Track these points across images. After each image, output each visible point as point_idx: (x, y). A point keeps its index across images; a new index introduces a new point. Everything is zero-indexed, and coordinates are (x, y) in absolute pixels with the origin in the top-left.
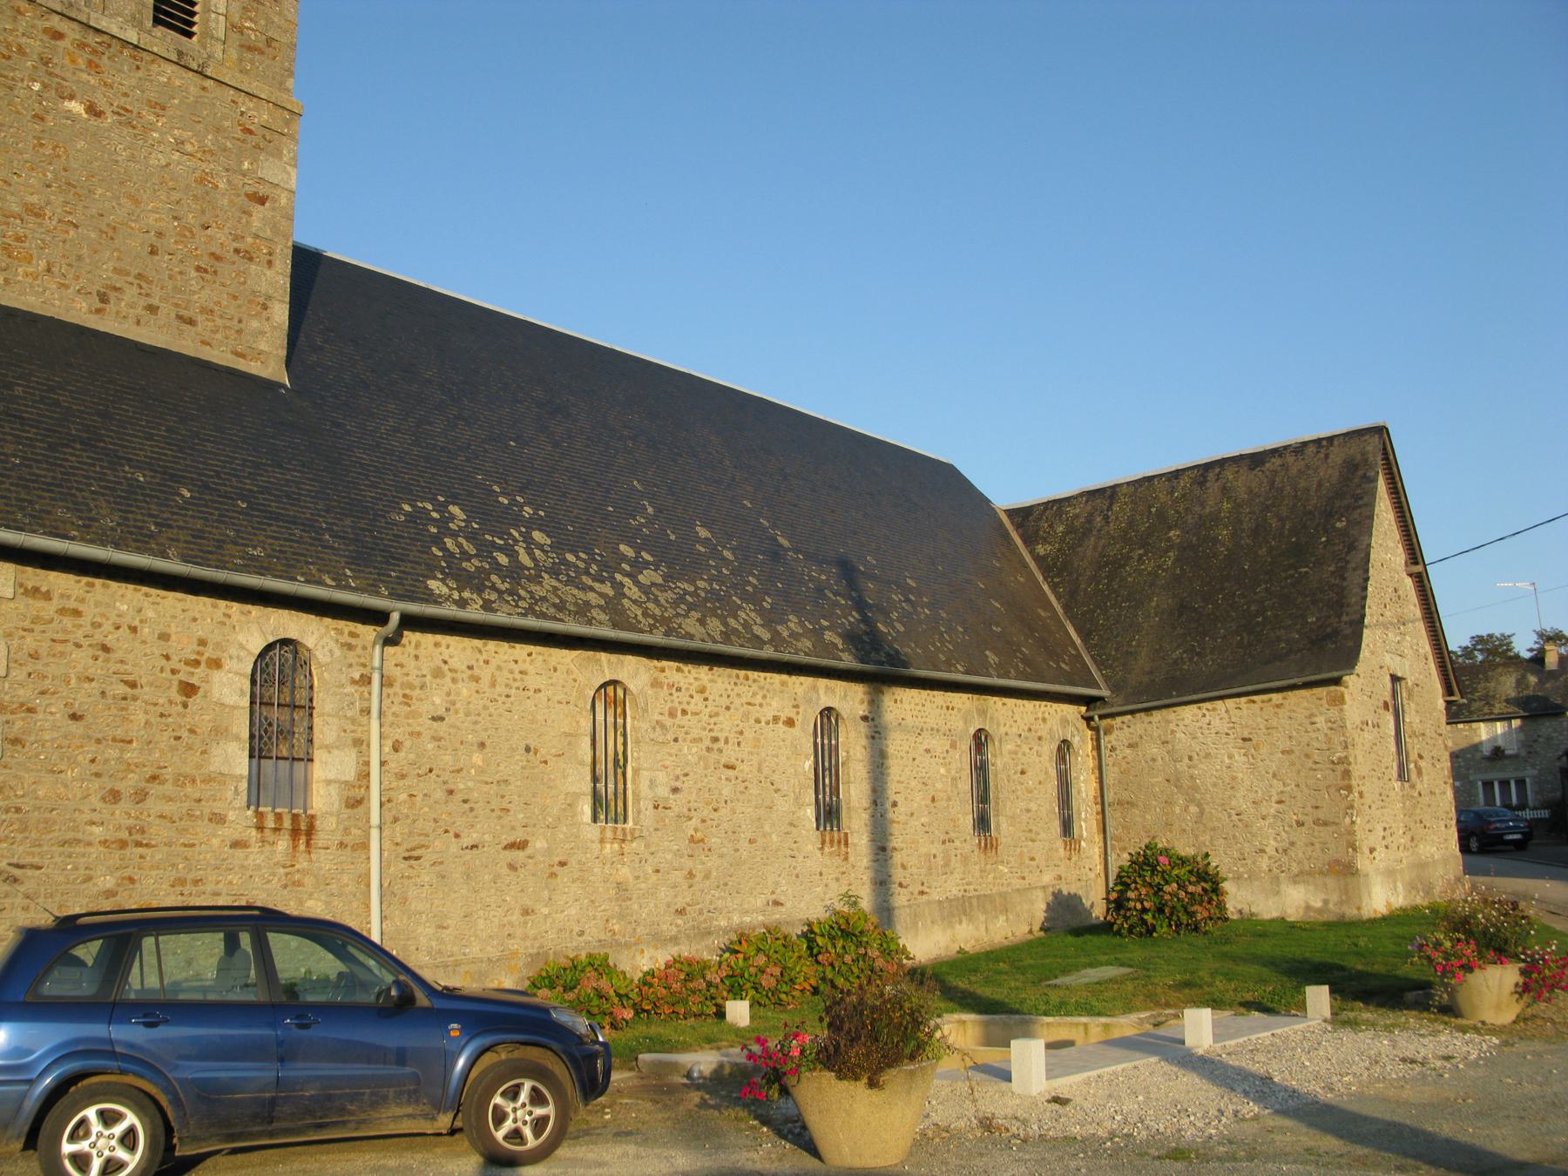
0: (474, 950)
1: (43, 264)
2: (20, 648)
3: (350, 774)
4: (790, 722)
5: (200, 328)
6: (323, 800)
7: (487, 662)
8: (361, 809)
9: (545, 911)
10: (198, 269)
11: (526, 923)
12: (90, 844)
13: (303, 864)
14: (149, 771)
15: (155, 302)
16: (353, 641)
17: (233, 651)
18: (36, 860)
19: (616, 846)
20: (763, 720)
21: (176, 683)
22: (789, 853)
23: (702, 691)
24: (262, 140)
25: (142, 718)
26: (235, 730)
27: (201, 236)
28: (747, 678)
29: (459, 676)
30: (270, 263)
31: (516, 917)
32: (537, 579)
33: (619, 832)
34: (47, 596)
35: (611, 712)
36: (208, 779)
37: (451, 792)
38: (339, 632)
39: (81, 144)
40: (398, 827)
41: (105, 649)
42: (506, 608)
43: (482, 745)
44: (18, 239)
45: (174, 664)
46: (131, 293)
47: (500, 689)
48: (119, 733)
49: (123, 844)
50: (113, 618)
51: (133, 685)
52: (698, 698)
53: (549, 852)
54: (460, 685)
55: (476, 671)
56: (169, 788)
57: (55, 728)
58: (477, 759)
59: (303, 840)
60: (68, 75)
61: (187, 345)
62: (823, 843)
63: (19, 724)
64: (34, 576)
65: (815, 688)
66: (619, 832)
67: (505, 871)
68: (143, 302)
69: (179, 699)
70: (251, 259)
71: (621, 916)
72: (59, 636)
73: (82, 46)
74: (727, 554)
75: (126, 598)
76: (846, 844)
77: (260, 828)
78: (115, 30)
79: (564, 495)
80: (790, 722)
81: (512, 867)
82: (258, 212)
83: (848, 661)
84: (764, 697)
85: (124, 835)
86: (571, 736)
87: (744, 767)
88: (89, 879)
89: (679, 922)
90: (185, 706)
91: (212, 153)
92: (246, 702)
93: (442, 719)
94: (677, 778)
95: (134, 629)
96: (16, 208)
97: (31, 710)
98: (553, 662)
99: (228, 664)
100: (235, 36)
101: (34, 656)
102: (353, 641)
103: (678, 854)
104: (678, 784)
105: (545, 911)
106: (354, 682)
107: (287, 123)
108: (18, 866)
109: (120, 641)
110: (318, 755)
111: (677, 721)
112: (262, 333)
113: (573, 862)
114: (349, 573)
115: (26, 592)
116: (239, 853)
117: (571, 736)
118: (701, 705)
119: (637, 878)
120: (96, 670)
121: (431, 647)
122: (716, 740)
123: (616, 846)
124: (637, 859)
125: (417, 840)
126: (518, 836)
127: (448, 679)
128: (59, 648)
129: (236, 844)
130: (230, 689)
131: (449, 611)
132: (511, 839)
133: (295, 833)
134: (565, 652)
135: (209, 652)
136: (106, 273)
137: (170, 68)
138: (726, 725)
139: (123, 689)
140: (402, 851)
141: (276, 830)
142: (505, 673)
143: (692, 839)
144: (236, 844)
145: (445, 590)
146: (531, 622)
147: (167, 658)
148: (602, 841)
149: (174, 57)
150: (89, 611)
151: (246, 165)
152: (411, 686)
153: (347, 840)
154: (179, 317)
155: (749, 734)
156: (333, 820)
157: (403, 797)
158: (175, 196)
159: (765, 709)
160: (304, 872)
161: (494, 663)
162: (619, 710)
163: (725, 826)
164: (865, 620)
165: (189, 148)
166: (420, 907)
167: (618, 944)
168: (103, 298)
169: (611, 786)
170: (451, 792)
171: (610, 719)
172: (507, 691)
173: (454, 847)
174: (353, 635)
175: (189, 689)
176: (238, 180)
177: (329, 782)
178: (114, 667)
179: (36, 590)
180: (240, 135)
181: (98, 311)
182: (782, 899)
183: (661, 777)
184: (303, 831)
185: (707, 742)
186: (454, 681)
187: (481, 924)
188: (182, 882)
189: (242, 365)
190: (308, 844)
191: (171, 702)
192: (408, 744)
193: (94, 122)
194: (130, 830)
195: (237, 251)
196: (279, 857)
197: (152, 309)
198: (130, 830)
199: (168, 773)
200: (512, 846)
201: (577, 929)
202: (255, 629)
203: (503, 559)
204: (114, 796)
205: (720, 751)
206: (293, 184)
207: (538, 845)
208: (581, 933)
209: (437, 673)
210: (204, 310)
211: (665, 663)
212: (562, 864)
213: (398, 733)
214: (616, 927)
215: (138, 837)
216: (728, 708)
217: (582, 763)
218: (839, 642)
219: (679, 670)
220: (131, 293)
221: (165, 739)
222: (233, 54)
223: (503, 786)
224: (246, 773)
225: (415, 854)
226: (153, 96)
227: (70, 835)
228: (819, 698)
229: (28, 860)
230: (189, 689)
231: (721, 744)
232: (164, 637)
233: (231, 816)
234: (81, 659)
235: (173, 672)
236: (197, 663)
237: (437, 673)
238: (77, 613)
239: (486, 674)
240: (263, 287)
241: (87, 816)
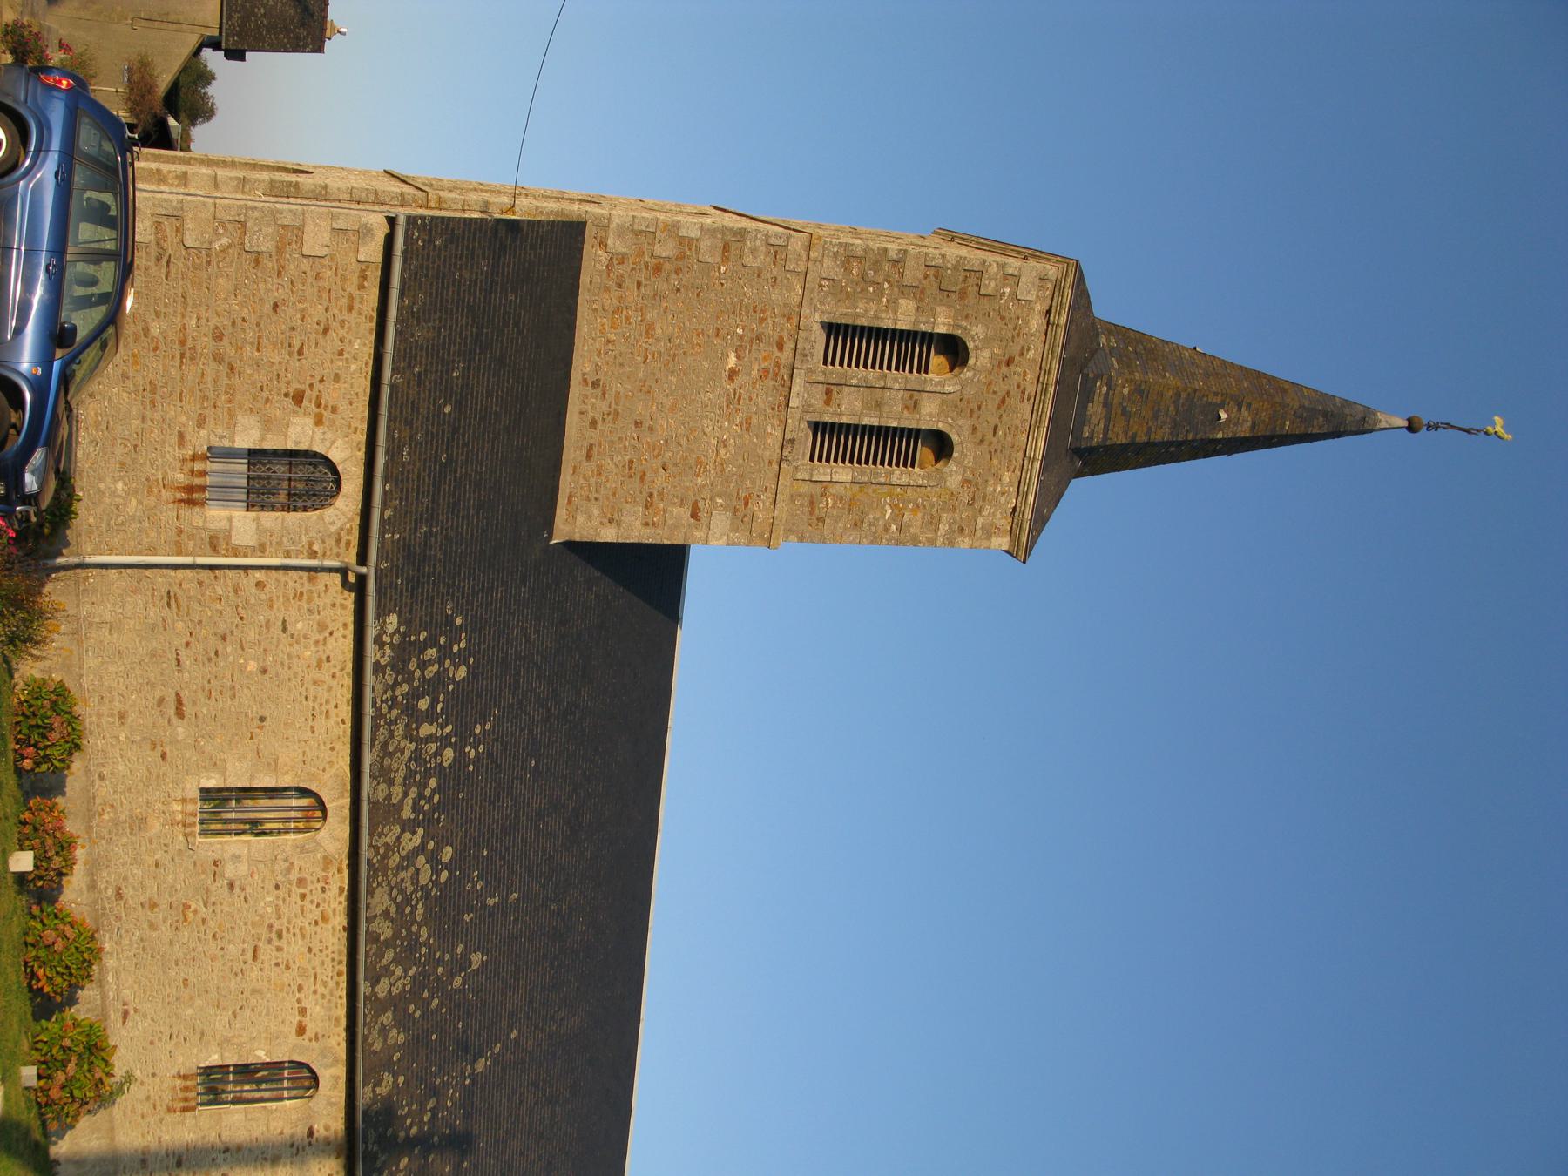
0: (91, 662)
1: (613, 337)
2: (323, 266)
3: (238, 539)
4: (301, 1030)
5: (585, 464)
6: (216, 515)
7: (334, 676)
8: (208, 549)
9: (122, 738)
10: (631, 462)
11: (112, 715)
12: (183, 316)
13: (166, 495)
14: (237, 365)
15: (600, 426)
16: (343, 545)
17: (329, 435)
18: (172, 275)
19: (179, 817)
20: (302, 995)
21: (302, 387)
22: (175, 1031)
23: (325, 918)
24: (742, 517)
25: (277, 359)
26: (269, 436)
27: (657, 464)
28: (339, 974)
29: (321, 647)
30: (647, 524)
31: (118, 706)
32: (409, 735)
33: (192, 819)
34: (361, 287)
35: (299, 815)
36: (231, 414)
37: (224, 638)
38: (349, 532)
39: (706, 365)
40: (194, 585)
41: (326, 331)
42: (379, 688)
43: (264, 671)
44: (627, 319)
45: (317, 386)
46: (603, 406)
47: (312, 691)
48: (265, 341)
49: (183, 343)
50: (348, 337)
51: (300, 353)
52: (317, 914)
53: (174, 742)
54: (313, 648)
55: (325, 665)
56: (224, 381)
57: (268, 291)
58: (252, 666)
59: (185, 496)
60: (754, 355)
61: (571, 453)
62: (185, 1077)
63: (270, 265)
64: (375, 275)
65: (336, 1061)
66: (192, 819)
67: (158, 694)
68: (598, 416)
69: (291, 390)
70: (646, 507)
71: (116, 822)
72: (333, 295)
73: (778, 365)
74: (458, 982)
75: (363, 347)
76: (184, 1110)
77: (194, 458)
78: (795, 389)
79: (492, 803)
80: (301, 1030)
81: (161, 701)
82: (685, 512)
83: (365, 1094)
84: (323, 996)
85: (190, 343)
86: (274, 766)
87: (255, 974)
88: (157, 315)
89: (110, 892)
90: (286, 395)
91: (723, 471)
92: (291, 446)
93: (284, 630)
94: (243, 889)
95: (341, 353)
96: (649, 316)
97: (279, 273)
98: (338, 746)
99: (319, 431)
100: (818, 489)
101: (318, 277)
102: (343, 545)
103: (173, 890)
104: (237, 890)
105: (122, 738)
106: (311, 544)
107: (761, 536)
108: (168, 262)
109: (331, 343)
110: (252, 515)
111: (294, 888)
112: (590, 518)
113: (166, 768)
114: (397, 536)
115: (363, 271)
116: (174, 439)
117: (274, 766)
118: (311, 917)
119: (151, 842)
120: (310, 324)
121: (342, 619)
122: (280, 936)
123: (179, 817)
124: (168, 841)
125: (184, 604)
126: (188, 710)
127: (318, 636)
128: (325, 296)
129: (181, 436)
130: (300, 433)
131: (371, 631)
132: (185, 702)
133: (190, 489)
134: (348, 759)
135: (327, 415)
136: (615, 387)
137: (779, 433)
138: (294, 948)
139: (297, 344)
140: (176, 588)
141: (192, 472)
142: (326, 695)
143: (186, 907)
144: (181, 436)
145: (390, 629)
146: (369, 711)
147: (322, 381)
148: (184, 800)
149: (788, 436)
150: (352, 318)
151: (719, 501)
152: (309, 601)
153: (184, 536)
154: (591, 447)
155: (287, 977)
156: (200, 524)
157: (219, 591)
158: (684, 441)
159: (311, 997)
160: (159, 497)
161: (334, 683)
162: (301, 825)
163: (200, 948)
164: (410, 1143)
165: (722, 451)
166: (129, 607)
167: (90, 819)
168: (595, 384)
169: (233, 815)
170: (224, 638)
171: (293, 814)
172: (311, 698)
173: (178, 642)
174: (348, 543)
175: (298, 398)
176: (706, 493)
177: (230, 519)
178: (313, 337)
179: (364, 278)
180: (742, 494)
181: (585, 381)
182: (129, 1023)
183: (243, 869)
184: (192, 496)
185: (276, 926)
186: (317, 642)
187: (112, 668)
188: (153, 391)
189: (562, 501)
190: (180, 501)
191: (288, 383)
192: (263, 596)
193: (725, 375)
194: (193, 348)
195: (651, 495)
196: (170, 474)
197: (594, 424)
198: (193, 348)
199: (236, 381)
200: (179, 702)
201: (106, 771)
202: (345, 453)
203: (424, 704)
204: (218, 336)
205: (270, 941)
206: (713, 542)
207: (180, 730)
208: (101, 777)
209: (322, 627)
210: (600, 467)
211: (346, 873)
212: (163, 756)
213: (271, 587)
214: (106, 817)
215: (188, 355)
216: (310, 950)
217: (252, 777)
218: (382, 1090)
219: (341, 889)
220: (603, 406)
221: (260, 377)
222: (805, 488)
223: (229, 693)
224: (237, 445)
225: (173, 603)
226: (755, 420)
227: (190, 303)
228: (327, 1067)
229: (173, 270)
230: (298, 398)
231: (276, 943)
232: (337, 378)
233: (203, 433)
234: (317, 312)
235: (311, 385)
236: (318, 405)
237: (322, 627)
238: (350, 309)
239: (324, 675)
240: (626, 519)
241: (204, 315)
